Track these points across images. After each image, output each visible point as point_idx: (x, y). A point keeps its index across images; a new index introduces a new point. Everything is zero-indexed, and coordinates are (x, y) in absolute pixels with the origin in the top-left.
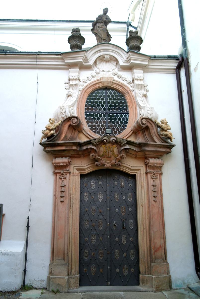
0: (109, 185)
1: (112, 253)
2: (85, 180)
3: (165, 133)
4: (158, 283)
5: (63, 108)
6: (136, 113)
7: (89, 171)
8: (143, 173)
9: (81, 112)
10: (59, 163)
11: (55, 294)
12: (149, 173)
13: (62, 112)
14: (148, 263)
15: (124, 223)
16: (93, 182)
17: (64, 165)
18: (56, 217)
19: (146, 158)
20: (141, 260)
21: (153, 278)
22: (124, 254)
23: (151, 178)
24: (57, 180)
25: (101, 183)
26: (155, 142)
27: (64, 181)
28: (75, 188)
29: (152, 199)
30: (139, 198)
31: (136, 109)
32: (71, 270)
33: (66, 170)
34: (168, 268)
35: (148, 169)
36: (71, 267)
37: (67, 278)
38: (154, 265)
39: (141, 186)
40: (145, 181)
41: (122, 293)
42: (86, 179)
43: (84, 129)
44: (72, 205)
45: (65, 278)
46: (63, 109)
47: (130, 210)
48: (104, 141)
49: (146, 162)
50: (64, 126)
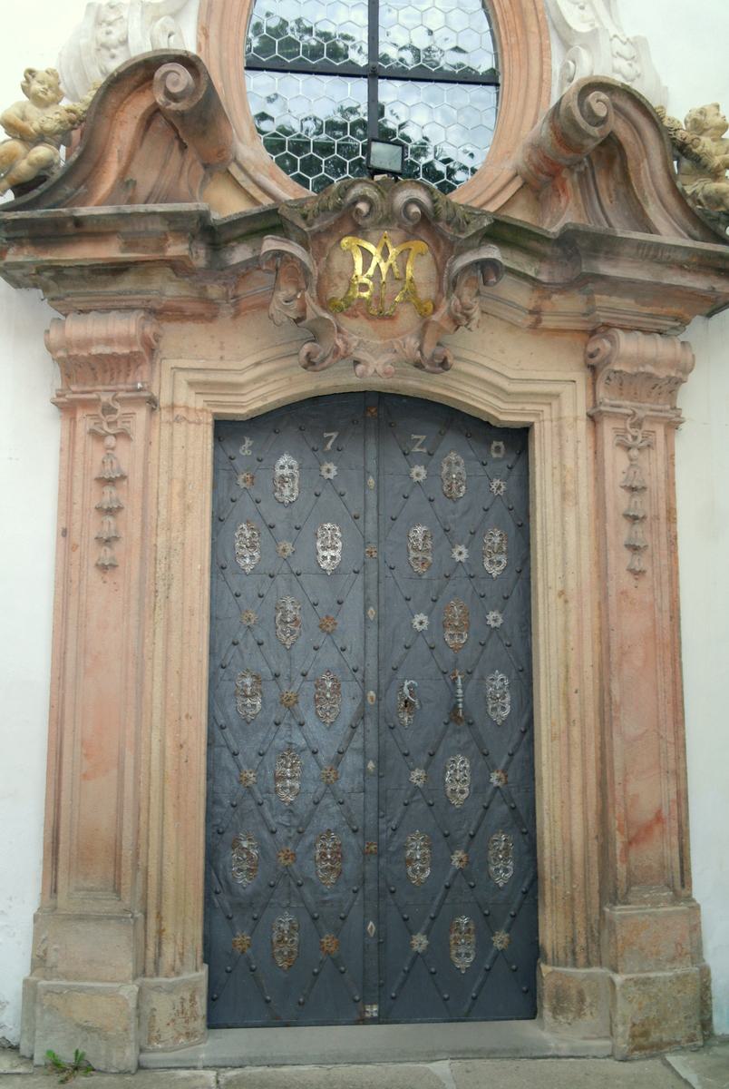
0: (378, 482)
1: (391, 849)
2: (246, 449)
3: (711, 186)
4: (640, 1009)
5: (112, 17)
6: (545, 77)
7: (263, 397)
8: (576, 419)
9: (225, 55)
10: (88, 343)
11: (62, 1082)
12: (607, 412)
13: (103, 38)
14: (587, 905)
15: (460, 691)
16: (286, 464)
17: (113, 356)
18: (70, 656)
19: (596, 331)
20: (552, 889)
21: (618, 988)
22: (458, 858)
23: (618, 445)
24: (79, 448)
25: (333, 468)
26: (650, 229)
27: (117, 453)
28: (183, 494)
29: (620, 560)
30: (545, 556)
31: (544, 51)
32: (159, 945)
33: (129, 387)
34: (696, 928)
35: (601, 393)
36: (160, 932)
37: (137, 989)
38: (624, 917)
39: (558, 489)
40: (582, 462)
41: (442, 1068)
42: (249, 448)
43: (240, 159)
44: (161, 589)
45: (121, 993)
46: (110, 24)
47: (495, 620)
48: (358, 211)
49: (592, 356)
50: (113, 117)
